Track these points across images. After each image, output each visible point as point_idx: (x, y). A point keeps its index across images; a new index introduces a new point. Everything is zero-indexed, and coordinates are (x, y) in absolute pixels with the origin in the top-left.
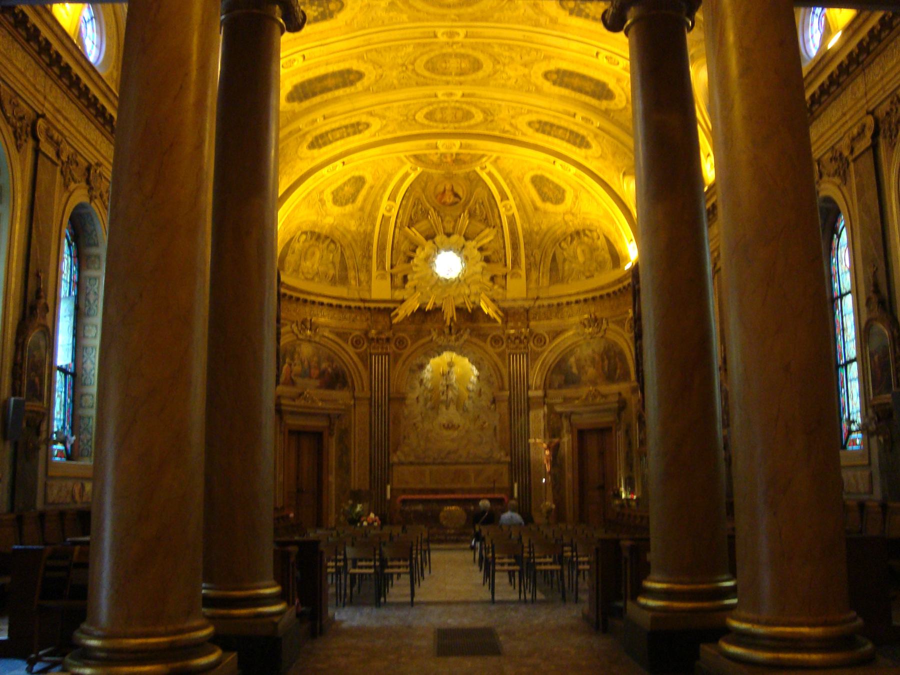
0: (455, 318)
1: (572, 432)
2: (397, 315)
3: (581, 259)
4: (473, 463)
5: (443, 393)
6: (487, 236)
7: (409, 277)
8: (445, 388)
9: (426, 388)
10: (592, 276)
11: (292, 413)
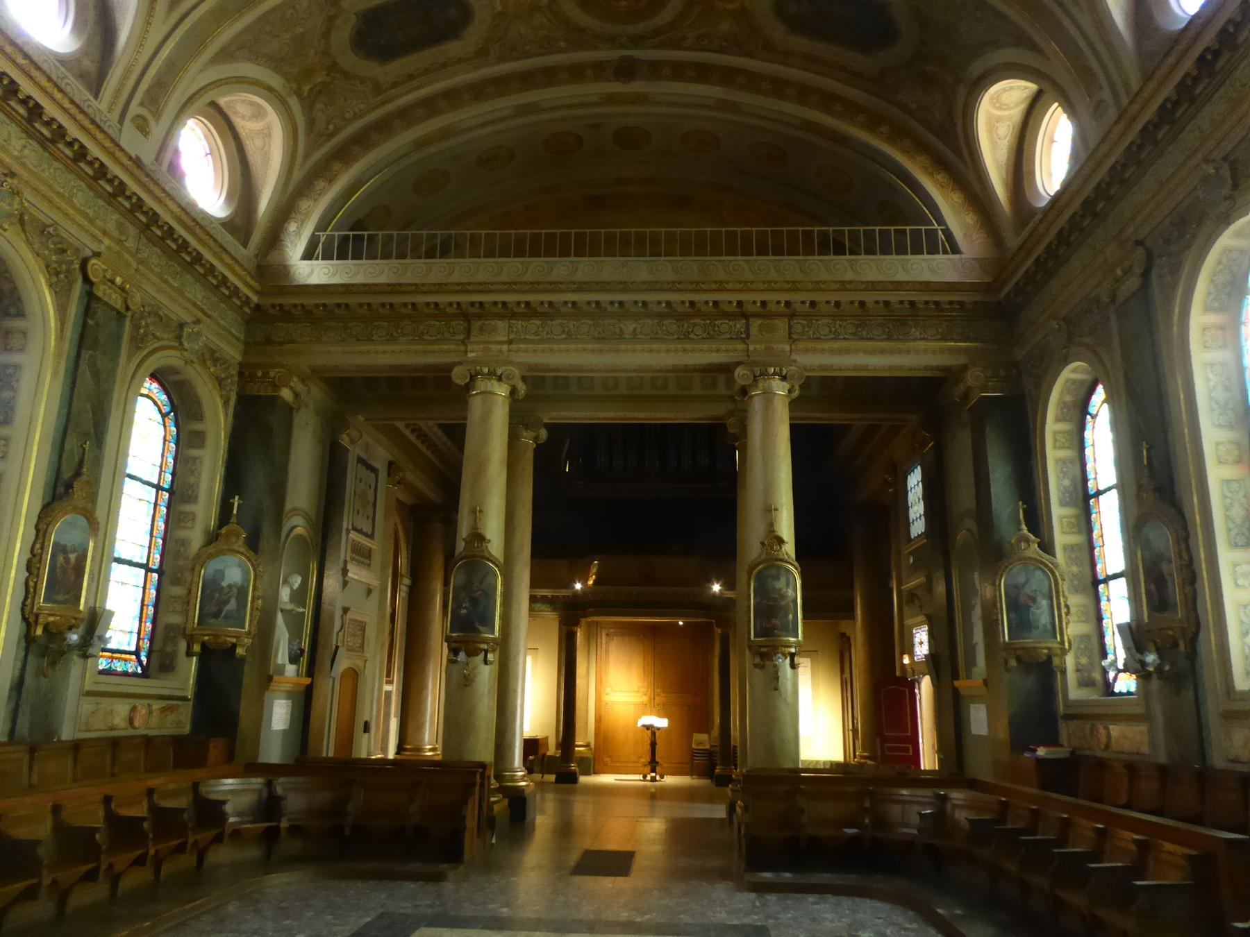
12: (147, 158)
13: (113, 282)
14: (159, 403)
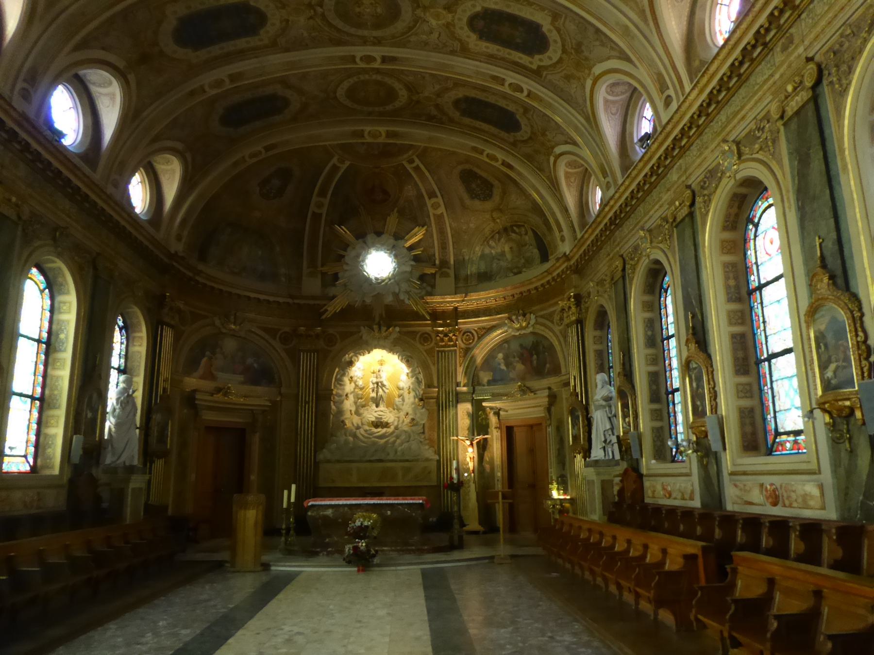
0: (384, 315)
1: (499, 428)
2: (326, 310)
3: (509, 256)
4: (401, 461)
5: (373, 391)
6: (415, 235)
7: (340, 275)
8: (376, 385)
9: (356, 386)
10: (520, 272)
11: (210, 408)
12: (31, 114)
13: (10, 200)
14: (38, 282)
